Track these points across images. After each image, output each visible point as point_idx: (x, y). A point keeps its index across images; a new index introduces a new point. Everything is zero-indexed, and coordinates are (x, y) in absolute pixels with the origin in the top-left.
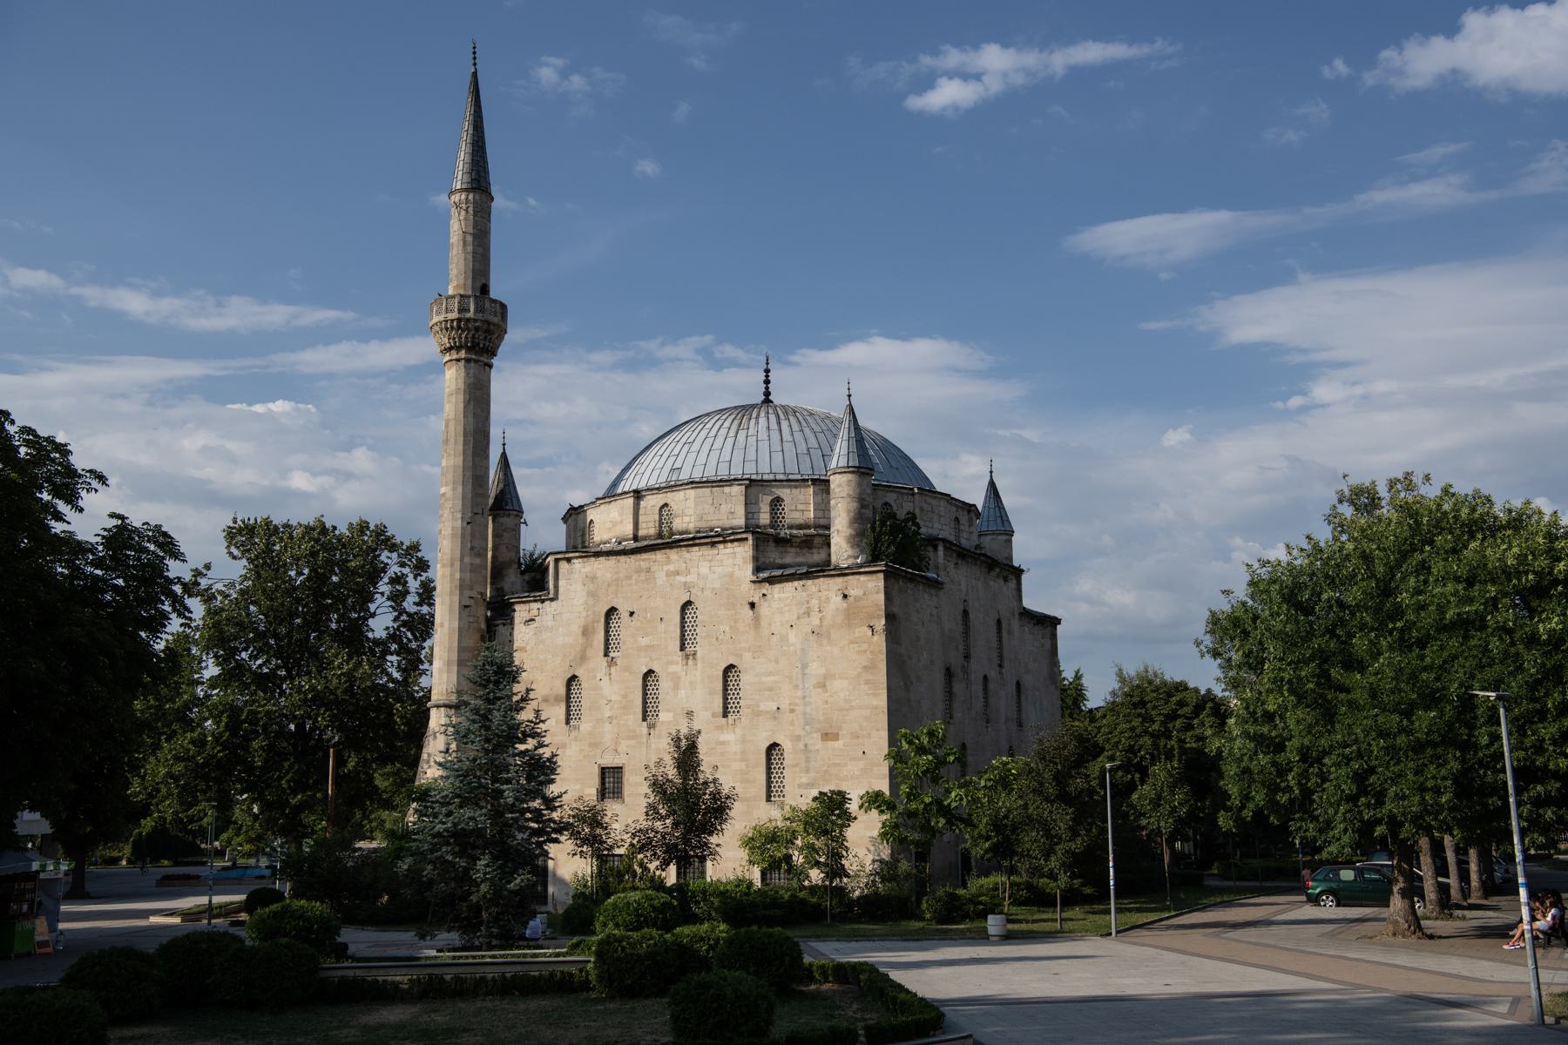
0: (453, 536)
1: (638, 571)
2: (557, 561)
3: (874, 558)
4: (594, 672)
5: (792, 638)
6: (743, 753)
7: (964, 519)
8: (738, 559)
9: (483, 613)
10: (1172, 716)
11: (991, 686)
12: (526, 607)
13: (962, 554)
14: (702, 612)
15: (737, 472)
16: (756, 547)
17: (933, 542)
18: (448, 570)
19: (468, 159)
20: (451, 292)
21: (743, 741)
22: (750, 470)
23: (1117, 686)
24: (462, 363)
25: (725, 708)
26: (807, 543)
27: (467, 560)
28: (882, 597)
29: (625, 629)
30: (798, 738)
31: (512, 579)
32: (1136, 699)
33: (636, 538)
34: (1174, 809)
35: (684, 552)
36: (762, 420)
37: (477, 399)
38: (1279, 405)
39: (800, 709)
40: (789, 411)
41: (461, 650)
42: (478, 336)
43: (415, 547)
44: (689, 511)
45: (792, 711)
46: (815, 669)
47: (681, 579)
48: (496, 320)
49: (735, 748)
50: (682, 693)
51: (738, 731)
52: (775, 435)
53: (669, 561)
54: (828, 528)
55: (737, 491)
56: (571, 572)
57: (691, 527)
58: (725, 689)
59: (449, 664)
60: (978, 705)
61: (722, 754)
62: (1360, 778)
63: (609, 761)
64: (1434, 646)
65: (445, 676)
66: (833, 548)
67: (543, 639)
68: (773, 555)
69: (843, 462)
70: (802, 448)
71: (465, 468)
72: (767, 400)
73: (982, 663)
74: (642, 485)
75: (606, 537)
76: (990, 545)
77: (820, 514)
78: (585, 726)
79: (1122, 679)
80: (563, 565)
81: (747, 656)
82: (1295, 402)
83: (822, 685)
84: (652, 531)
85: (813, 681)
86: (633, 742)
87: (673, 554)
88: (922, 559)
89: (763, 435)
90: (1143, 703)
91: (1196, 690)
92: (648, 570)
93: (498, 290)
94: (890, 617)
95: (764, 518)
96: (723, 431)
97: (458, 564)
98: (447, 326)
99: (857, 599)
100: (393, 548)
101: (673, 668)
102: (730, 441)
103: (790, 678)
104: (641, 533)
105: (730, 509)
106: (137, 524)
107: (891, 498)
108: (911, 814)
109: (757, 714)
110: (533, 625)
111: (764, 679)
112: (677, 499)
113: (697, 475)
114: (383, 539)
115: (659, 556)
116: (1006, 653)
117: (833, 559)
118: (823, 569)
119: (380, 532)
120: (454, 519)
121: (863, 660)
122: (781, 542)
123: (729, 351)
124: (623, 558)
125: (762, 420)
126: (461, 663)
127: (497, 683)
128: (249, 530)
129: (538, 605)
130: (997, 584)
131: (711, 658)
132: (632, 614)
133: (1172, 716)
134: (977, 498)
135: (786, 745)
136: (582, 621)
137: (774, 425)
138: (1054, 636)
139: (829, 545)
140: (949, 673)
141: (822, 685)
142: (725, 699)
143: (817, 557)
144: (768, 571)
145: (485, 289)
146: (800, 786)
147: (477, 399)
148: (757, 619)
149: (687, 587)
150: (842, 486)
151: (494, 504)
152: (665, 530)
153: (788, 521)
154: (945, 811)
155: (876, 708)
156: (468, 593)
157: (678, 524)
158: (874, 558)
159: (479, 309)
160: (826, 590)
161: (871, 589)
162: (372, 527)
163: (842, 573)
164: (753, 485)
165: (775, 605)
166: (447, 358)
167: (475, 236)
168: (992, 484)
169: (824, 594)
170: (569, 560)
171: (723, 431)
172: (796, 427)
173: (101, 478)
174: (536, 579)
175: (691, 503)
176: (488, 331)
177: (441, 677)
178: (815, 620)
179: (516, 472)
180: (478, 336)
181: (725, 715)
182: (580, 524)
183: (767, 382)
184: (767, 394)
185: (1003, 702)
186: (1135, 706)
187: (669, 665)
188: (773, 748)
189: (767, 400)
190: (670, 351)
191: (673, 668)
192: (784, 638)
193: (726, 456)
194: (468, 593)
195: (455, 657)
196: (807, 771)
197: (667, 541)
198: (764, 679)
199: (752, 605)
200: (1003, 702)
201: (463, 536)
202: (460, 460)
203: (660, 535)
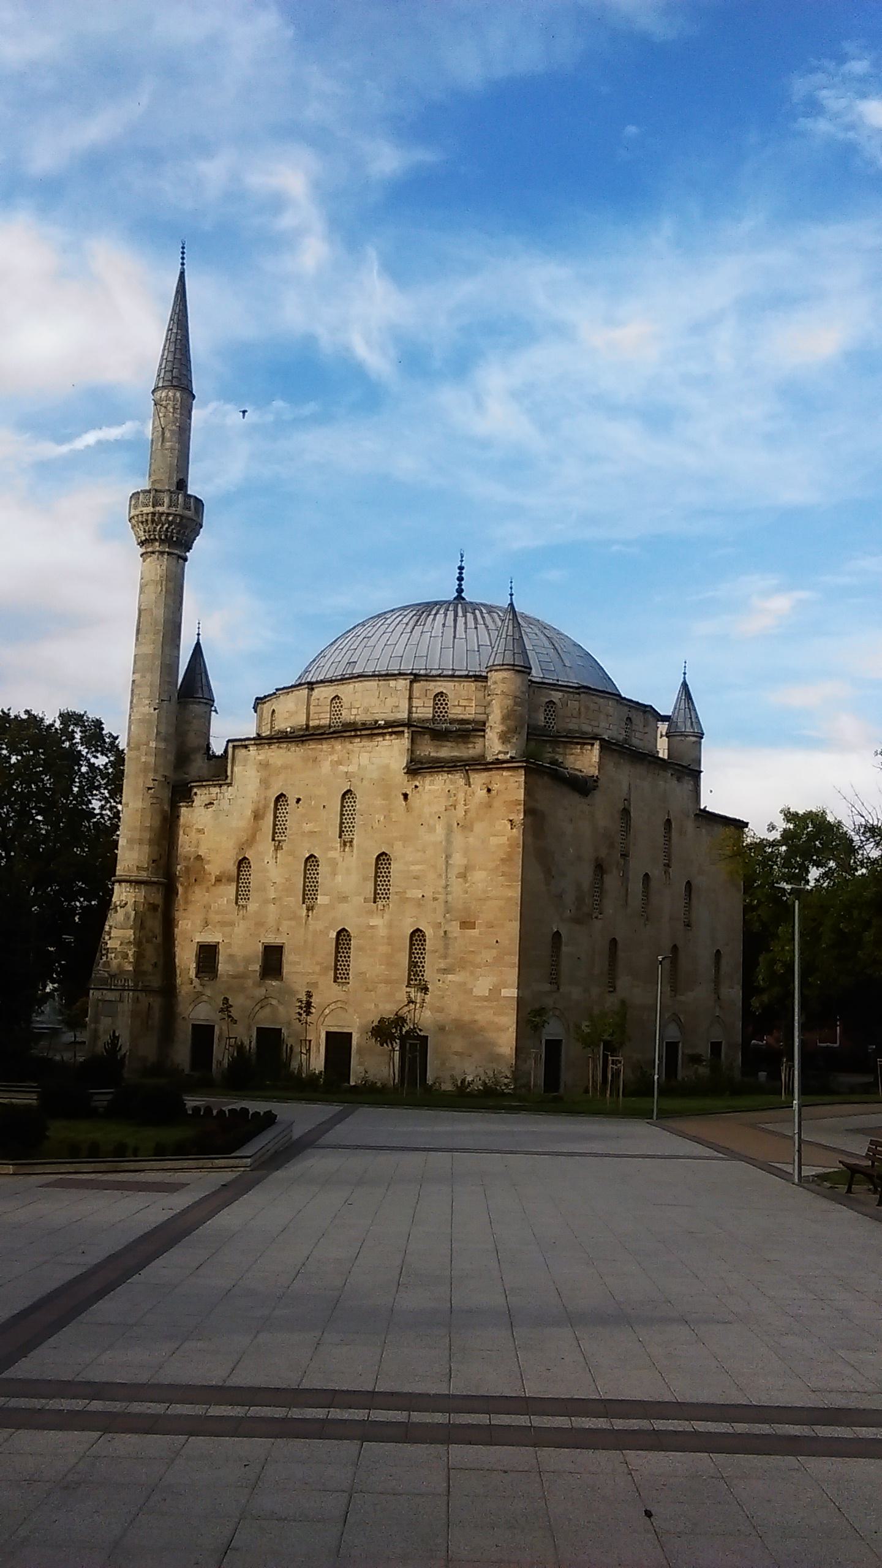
4: (263, 854)
9: (166, 794)
11: (654, 884)
15: (406, 667)
21: (390, 926)
24: (155, 556)
29: (292, 816)
31: (198, 765)
36: (440, 617)
45: (435, 899)
46: (458, 860)
49: (382, 932)
50: (339, 878)
51: (386, 916)
55: (402, 684)
56: (246, 760)
60: (636, 901)
61: (372, 938)
63: (272, 939)
67: (212, 826)
68: (429, 750)
72: (459, 597)
74: (314, 680)
77: (481, 710)
78: (252, 906)
81: (398, 845)
83: (463, 876)
86: (293, 923)
92: (315, 760)
93: (194, 489)
94: (530, 811)
101: (332, 854)
102: (406, 636)
103: (434, 867)
109: (405, 900)
111: (412, 868)
112: (346, 691)
118: (480, 764)
122: (439, 735)
128: (595, 788)
129: (217, 790)
131: (366, 845)
132: (298, 800)
135: (429, 932)
140: (600, 868)
145: (182, 485)
146: (439, 971)
150: (502, 682)
155: (510, 899)
161: (512, 786)
168: (685, 685)
178: (460, 812)
183: (460, 579)
184: (460, 591)
185: (668, 901)
187: (330, 853)
188: (417, 935)
189: (459, 597)
191: (332, 854)
196: (445, 957)
198: (412, 868)
199: (406, 796)
200: (668, 901)
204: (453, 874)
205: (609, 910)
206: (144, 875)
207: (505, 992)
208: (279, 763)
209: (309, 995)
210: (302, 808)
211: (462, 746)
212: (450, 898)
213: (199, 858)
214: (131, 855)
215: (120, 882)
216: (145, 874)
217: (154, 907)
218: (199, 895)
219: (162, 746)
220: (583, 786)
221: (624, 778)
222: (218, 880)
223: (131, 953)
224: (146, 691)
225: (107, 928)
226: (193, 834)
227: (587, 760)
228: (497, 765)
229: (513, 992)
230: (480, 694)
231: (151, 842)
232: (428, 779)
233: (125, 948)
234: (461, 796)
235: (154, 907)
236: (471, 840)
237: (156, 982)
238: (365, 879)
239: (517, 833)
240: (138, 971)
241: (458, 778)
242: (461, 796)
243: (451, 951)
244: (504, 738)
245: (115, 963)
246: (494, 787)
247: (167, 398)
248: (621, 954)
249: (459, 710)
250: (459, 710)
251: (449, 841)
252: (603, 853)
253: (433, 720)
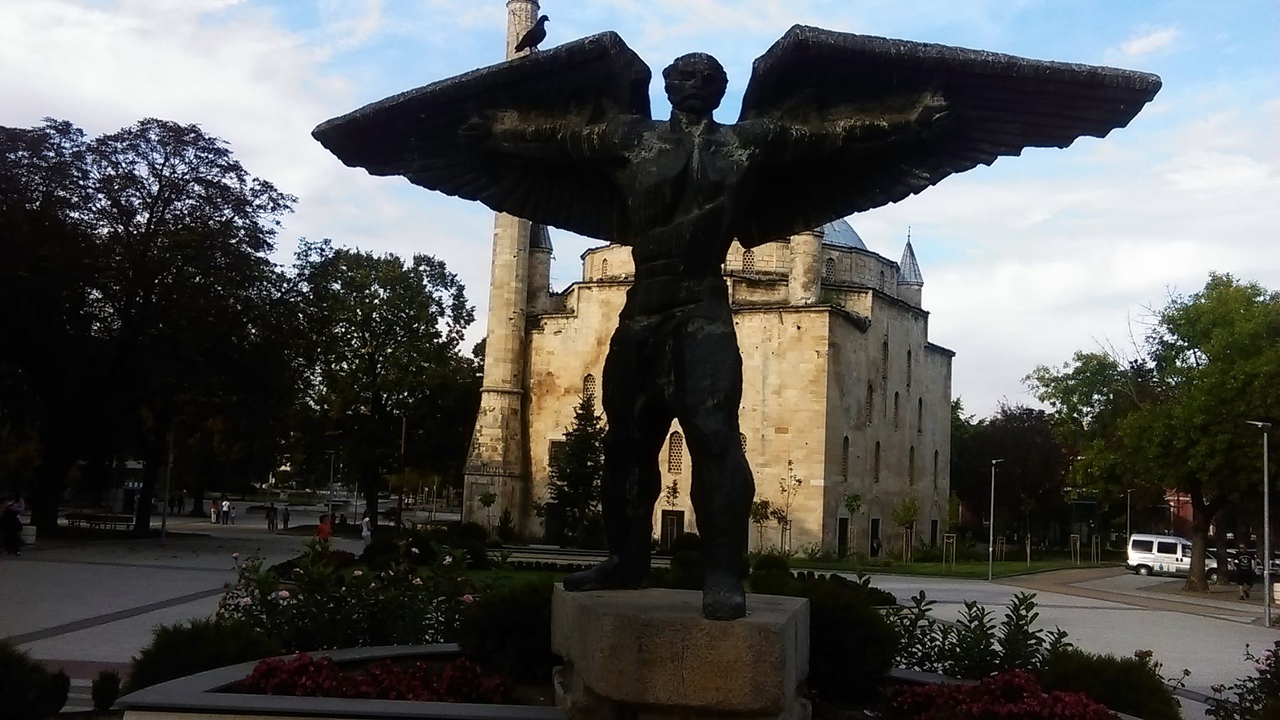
7: (888, 273)
9: (523, 324)
11: (901, 400)
12: (554, 322)
31: (543, 302)
56: (589, 299)
60: (891, 412)
76: (904, 293)
83: (778, 393)
110: (560, 336)
118: (783, 307)
129: (565, 321)
134: (896, 255)
138: (950, 364)
140: (871, 389)
161: (819, 324)
168: (909, 245)
178: (775, 343)
196: (763, 455)
200: (908, 413)
204: (769, 391)
205: (875, 421)
206: (508, 387)
207: (813, 482)
208: (124, 645)
209: (675, 484)
211: (770, 292)
212: (766, 410)
213: (549, 374)
214: (496, 372)
215: (488, 391)
216: (508, 385)
217: (515, 412)
218: (550, 403)
219: (520, 285)
220: (860, 325)
221: (886, 321)
222: (567, 391)
223: (499, 447)
224: (507, 242)
225: (478, 427)
226: (544, 355)
227: (862, 305)
228: (807, 308)
229: (821, 482)
230: (780, 252)
231: (512, 361)
232: (747, 317)
233: (495, 444)
234: (775, 332)
235: (515, 412)
236: (784, 365)
237: (517, 471)
239: (823, 361)
240: (506, 461)
241: (773, 318)
242: (775, 332)
244: (806, 287)
245: (485, 455)
246: (803, 325)
247: (521, 10)
248: (882, 453)
249: (762, 264)
250: (762, 264)
251: (765, 366)
252: (872, 377)
253: (743, 271)
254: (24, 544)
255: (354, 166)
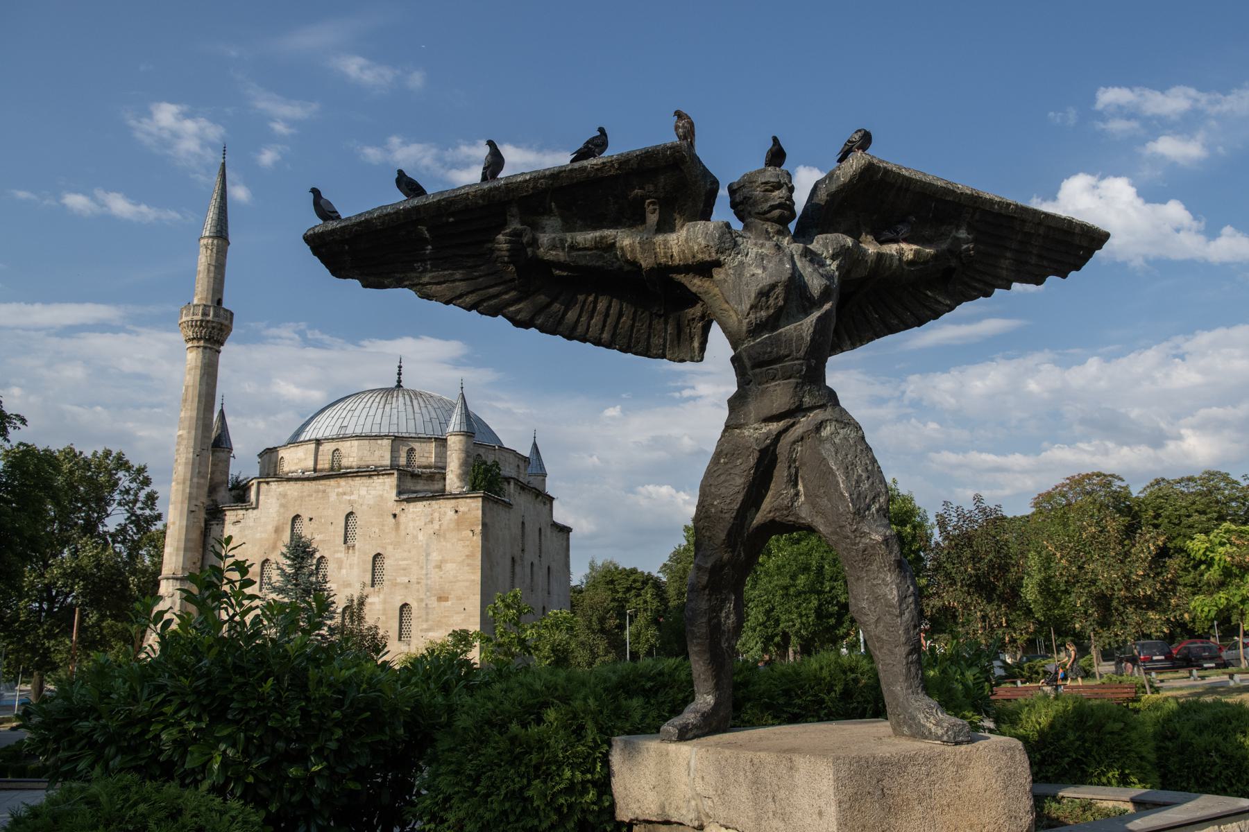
0: (186, 464)
1: (317, 491)
2: (259, 483)
3: (474, 488)
5: (421, 537)
6: (384, 610)
7: (522, 465)
8: (386, 487)
10: (628, 590)
11: (535, 569)
12: (234, 513)
13: (524, 487)
14: (360, 520)
15: (385, 431)
16: (399, 479)
17: (508, 480)
18: (181, 487)
19: (215, 217)
20: (195, 302)
21: (385, 602)
22: (394, 430)
23: (588, 571)
25: (373, 581)
26: (431, 477)
27: (195, 480)
28: (480, 512)
30: (422, 600)
31: (223, 495)
32: (608, 579)
33: (315, 470)
34: (648, 640)
35: (350, 481)
36: (401, 399)
37: (209, 373)
38: (677, 395)
39: (424, 582)
40: (417, 395)
41: (187, 540)
42: (213, 332)
43: (141, 470)
44: (353, 454)
46: (435, 556)
47: (347, 497)
48: (226, 323)
50: (344, 571)
51: (381, 596)
52: (410, 409)
53: (339, 486)
54: (444, 468)
55: (386, 443)
56: (269, 491)
57: (354, 464)
58: (374, 569)
59: (178, 549)
62: (768, 613)
64: (803, 543)
65: (174, 558)
66: (448, 482)
68: (410, 484)
69: (457, 428)
70: (427, 418)
71: (198, 419)
72: (399, 386)
73: (530, 556)
74: (319, 436)
75: (293, 468)
76: (534, 482)
79: (592, 567)
80: (264, 486)
81: (390, 548)
82: (686, 393)
83: (439, 567)
84: (327, 466)
85: (433, 564)
87: (342, 482)
88: (501, 489)
89: (402, 408)
90: (612, 582)
91: (642, 573)
92: (324, 491)
94: (484, 525)
95: (403, 461)
96: (375, 404)
97: (188, 483)
98: (192, 324)
99: (464, 513)
100: (128, 469)
102: (380, 411)
104: (319, 467)
105: (381, 454)
106: (1028, 510)
107: (482, 451)
108: (500, 645)
109: (395, 585)
110: (239, 525)
112: (345, 447)
113: (358, 431)
114: (122, 463)
115: (332, 482)
116: (544, 549)
117: (448, 488)
118: (441, 494)
119: (120, 457)
120: (188, 452)
121: (467, 551)
123: (317, 334)
124: (306, 483)
125: (401, 399)
126: (186, 550)
127: (303, 558)
130: (540, 506)
131: (365, 547)
133: (628, 590)
134: (526, 452)
136: (275, 524)
137: (408, 402)
138: (568, 539)
139: (445, 479)
141: (439, 567)
142: (373, 575)
143: (437, 486)
144: (407, 494)
145: (219, 302)
147: (209, 373)
148: (397, 525)
149: (351, 503)
150: (455, 445)
151: (215, 444)
152: (336, 466)
153: (417, 463)
154: (522, 642)
156: (194, 502)
157: (345, 462)
158: (474, 488)
159: (216, 315)
160: (444, 508)
161: (473, 507)
162: (114, 454)
163: (455, 497)
164: (397, 440)
165: (410, 516)
166: (190, 345)
167: (216, 267)
168: (535, 445)
169: (443, 510)
170: (268, 483)
171: (375, 404)
172: (422, 404)
173: (23, 421)
174: (241, 494)
175: (355, 449)
176: (221, 330)
177: (173, 559)
178: (437, 527)
179: (229, 421)
180: (213, 332)
181: (373, 585)
182: (274, 459)
183: (399, 374)
184: (399, 381)
186: (607, 583)
188: (404, 606)
189: (399, 386)
190: (274, 331)
192: (416, 537)
193: (378, 419)
194: (194, 502)
195: (182, 546)
196: (427, 621)
197: (336, 473)
199: (395, 516)
201: (193, 464)
202: (194, 414)
203: (332, 469)
210: (313, 524)
238: (365, 571)
243: (430, 617)
246: (461, 509)
254: (712, 276)
255: (345, 278)
